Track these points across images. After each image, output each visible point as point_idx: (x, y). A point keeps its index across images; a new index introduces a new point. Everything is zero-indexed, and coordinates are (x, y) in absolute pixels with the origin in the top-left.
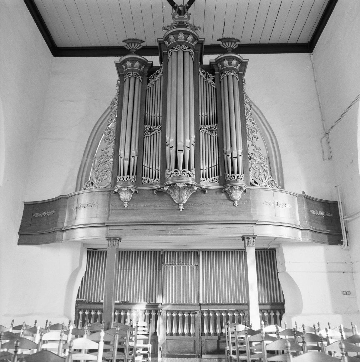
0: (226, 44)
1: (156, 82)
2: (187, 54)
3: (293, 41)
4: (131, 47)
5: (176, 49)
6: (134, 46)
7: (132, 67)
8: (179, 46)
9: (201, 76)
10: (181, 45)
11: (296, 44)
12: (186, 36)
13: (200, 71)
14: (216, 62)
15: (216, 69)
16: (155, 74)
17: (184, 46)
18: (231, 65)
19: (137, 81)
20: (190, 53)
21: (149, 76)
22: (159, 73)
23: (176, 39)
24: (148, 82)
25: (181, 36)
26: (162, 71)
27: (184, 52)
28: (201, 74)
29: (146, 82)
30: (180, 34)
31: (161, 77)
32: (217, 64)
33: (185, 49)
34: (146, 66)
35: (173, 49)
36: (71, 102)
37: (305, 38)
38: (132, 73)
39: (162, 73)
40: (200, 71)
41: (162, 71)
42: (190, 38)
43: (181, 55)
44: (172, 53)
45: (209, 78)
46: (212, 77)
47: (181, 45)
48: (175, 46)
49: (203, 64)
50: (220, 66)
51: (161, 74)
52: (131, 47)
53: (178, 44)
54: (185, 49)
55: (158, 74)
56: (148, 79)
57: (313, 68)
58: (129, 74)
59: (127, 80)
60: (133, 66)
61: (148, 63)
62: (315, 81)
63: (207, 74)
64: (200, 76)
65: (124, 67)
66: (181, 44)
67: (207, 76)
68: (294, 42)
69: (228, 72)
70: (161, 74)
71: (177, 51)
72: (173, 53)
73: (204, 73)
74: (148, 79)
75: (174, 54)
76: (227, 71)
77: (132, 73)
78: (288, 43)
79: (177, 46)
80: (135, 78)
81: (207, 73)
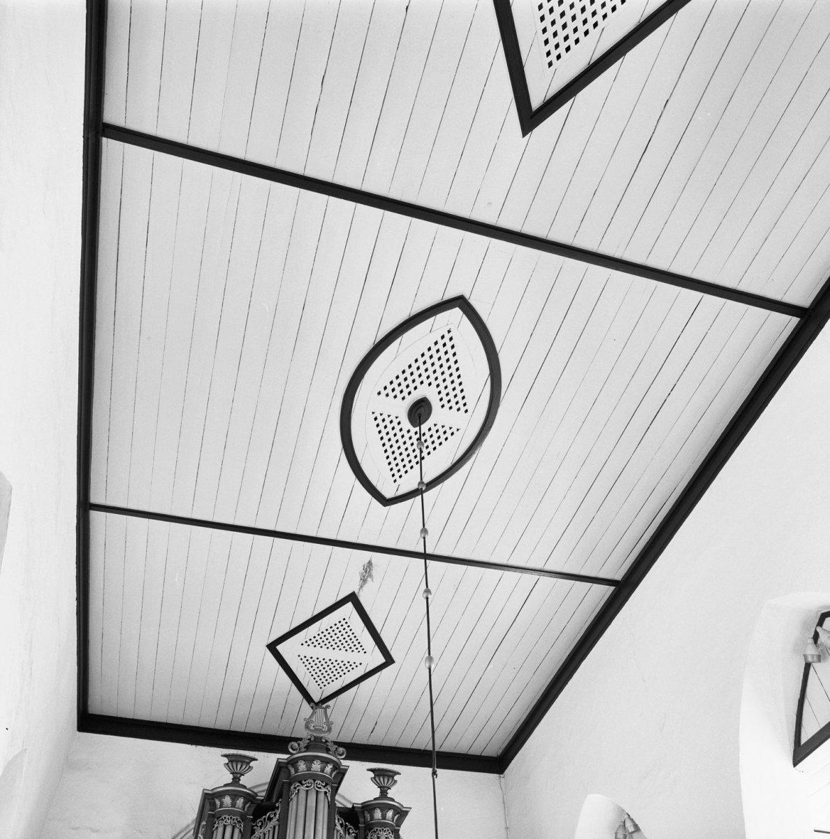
0: (379, 779)
1: (265, 834)
2: (322, 796)
3: (475, 751)
4: (235, 768)
5: (307, 787)
6: (241, 768)
7: (231, 807)
8: (312, 782)
9: (337, 831)
10: (315, 781)
11: (480, 756)
12: (325, 764)
13: (336, 821)
14: (363, 807)
15: (361, 820)
16: (265, 819)
17: (319, 782)
18: (385, 819)
19: (237, 831)
20: (326, 793)
21: (254, 820)
22: (272, 818)
23: (309, 769)
24: (253, 832)
25: (316, 766)
26: (277, 816)
27: (317, 791)
28: (338, 827)
29: (249, 833)
30: (315, 762)
31: (274, 827)
32: (363, 812)
33: (320, 788)
34: (252, 803)
35: (302, 785)
36: (94, 832)
37: (494, 750)
38: (231, 818)
39: (278, 820)
40: (336, 821)
41: (277, 816)
42: (329, 768)
43: (312, 797)
44: (298, 790)
45: (349, 833)
46: (353, 833)
47: (315, 781)
48: (305, 781)
49: (104, 140)
50: (368, 816)
51: (274, 822)
52: (235, 768)
53: (310, 778)
54: (320, 788)
55: (270, 819)
56: (253, 826)
57: (504, 803)
58: (225, 818)
59: (221, 830)
60: (233, 805)
61: (258, 798)
62: (507, 828)
63: (346, 826)
64: (335, 831)
65: (218, 803)
66: (314, 777)
67: (346, 830)
68: (478, 753)
69: (380, 831)
70: (274, 822)
71: (307, 791)
72: (300, 791)
73: (342, 825)
74: (253, 826)
75: (302, 795)
76: (379, 829)
77: (231, 818)
78: (469, 753)
79: (307, 781)
80: (234, 828)
81: (347, 823)
